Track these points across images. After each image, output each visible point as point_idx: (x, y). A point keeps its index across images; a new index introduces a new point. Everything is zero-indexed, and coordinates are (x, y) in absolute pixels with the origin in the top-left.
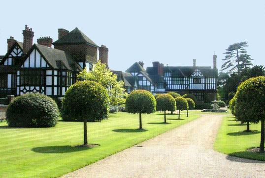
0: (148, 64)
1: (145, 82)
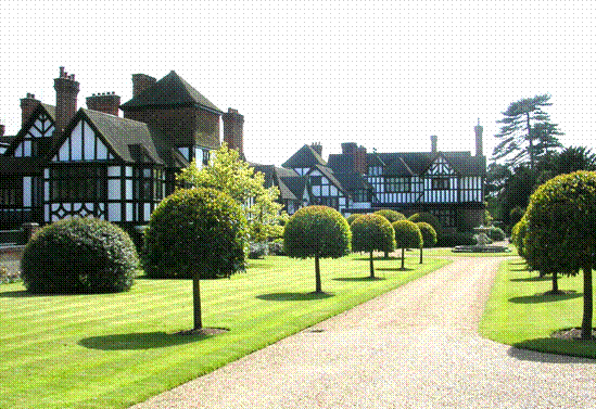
0: (331, 148)
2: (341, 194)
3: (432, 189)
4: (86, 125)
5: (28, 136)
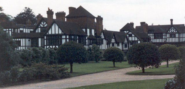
0: (137, 24)
1: (150, 35)
2: (138, 40)
3: (170, 38)
4: (56, 24)
5: (39, 26)
